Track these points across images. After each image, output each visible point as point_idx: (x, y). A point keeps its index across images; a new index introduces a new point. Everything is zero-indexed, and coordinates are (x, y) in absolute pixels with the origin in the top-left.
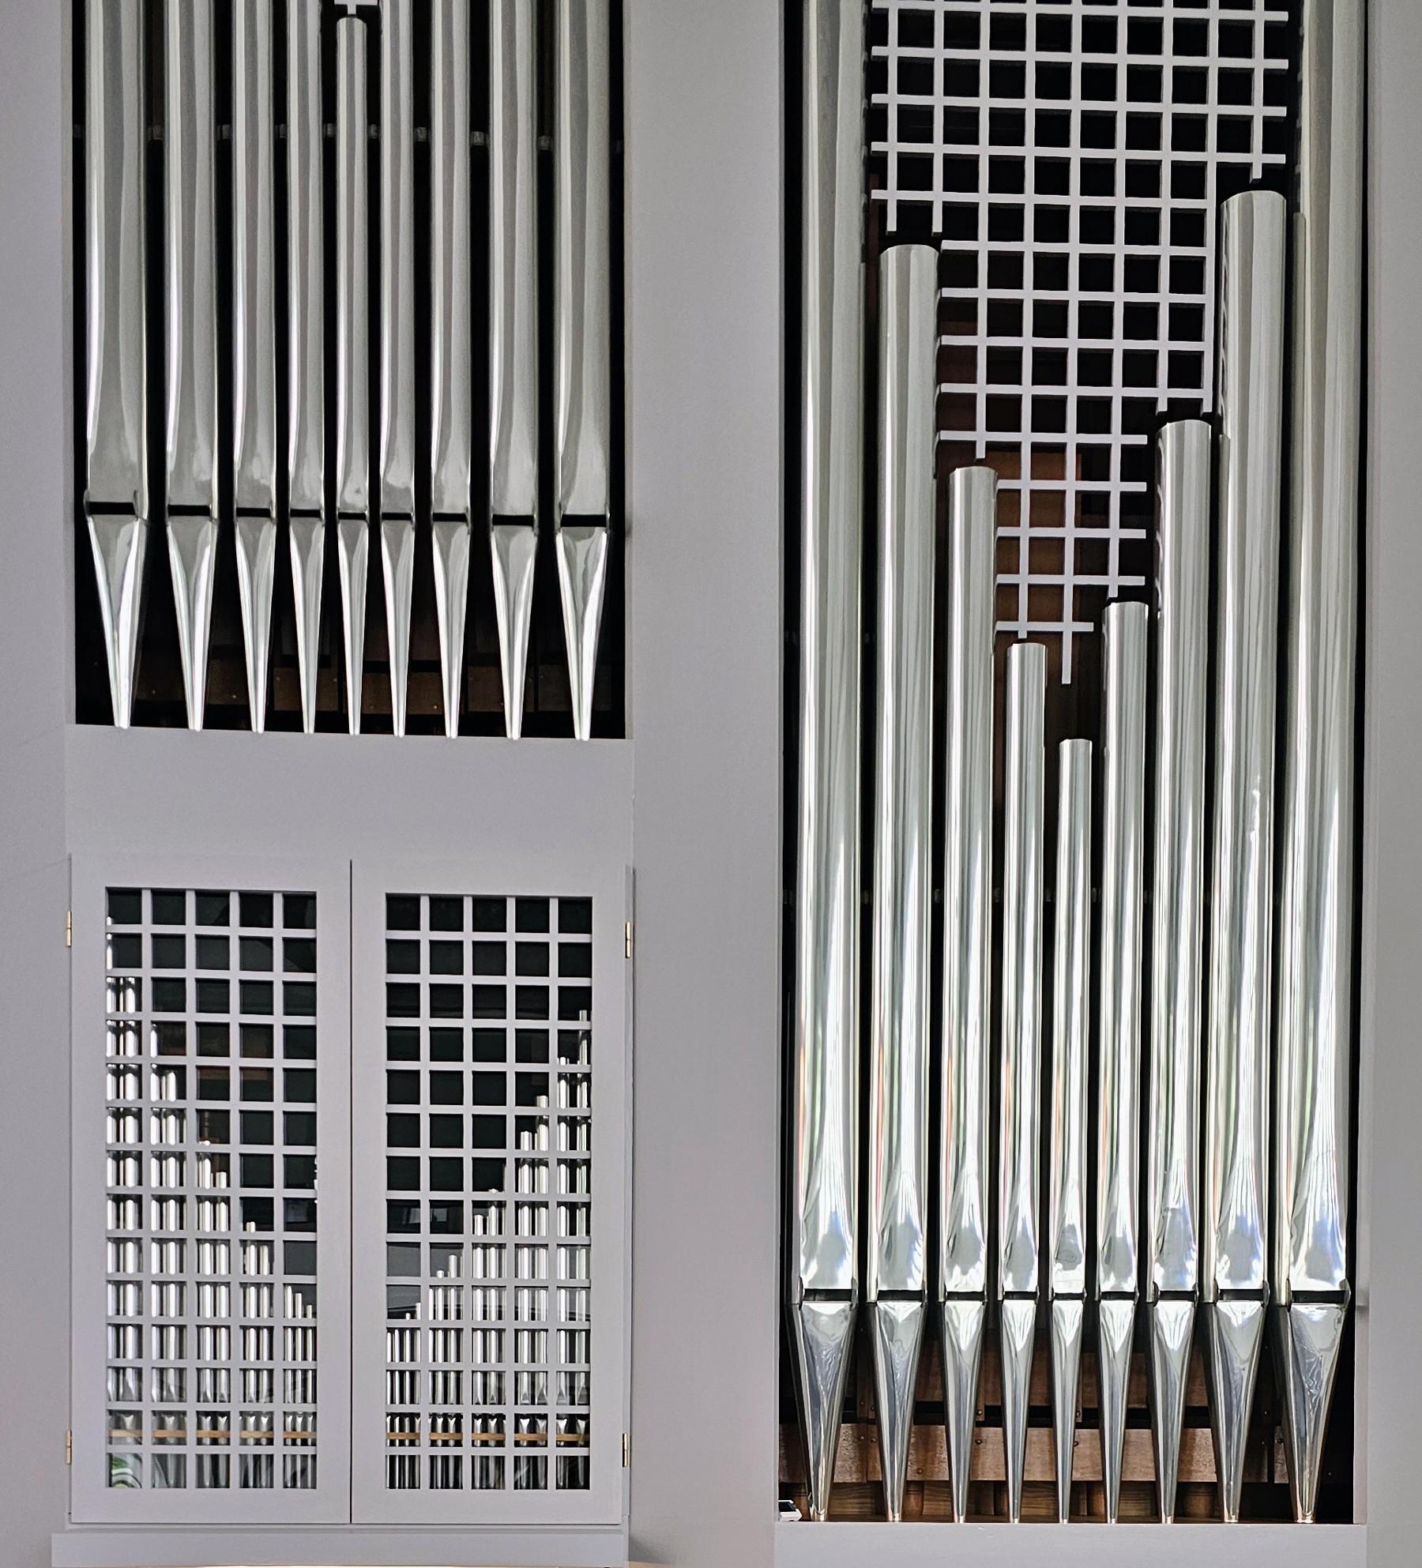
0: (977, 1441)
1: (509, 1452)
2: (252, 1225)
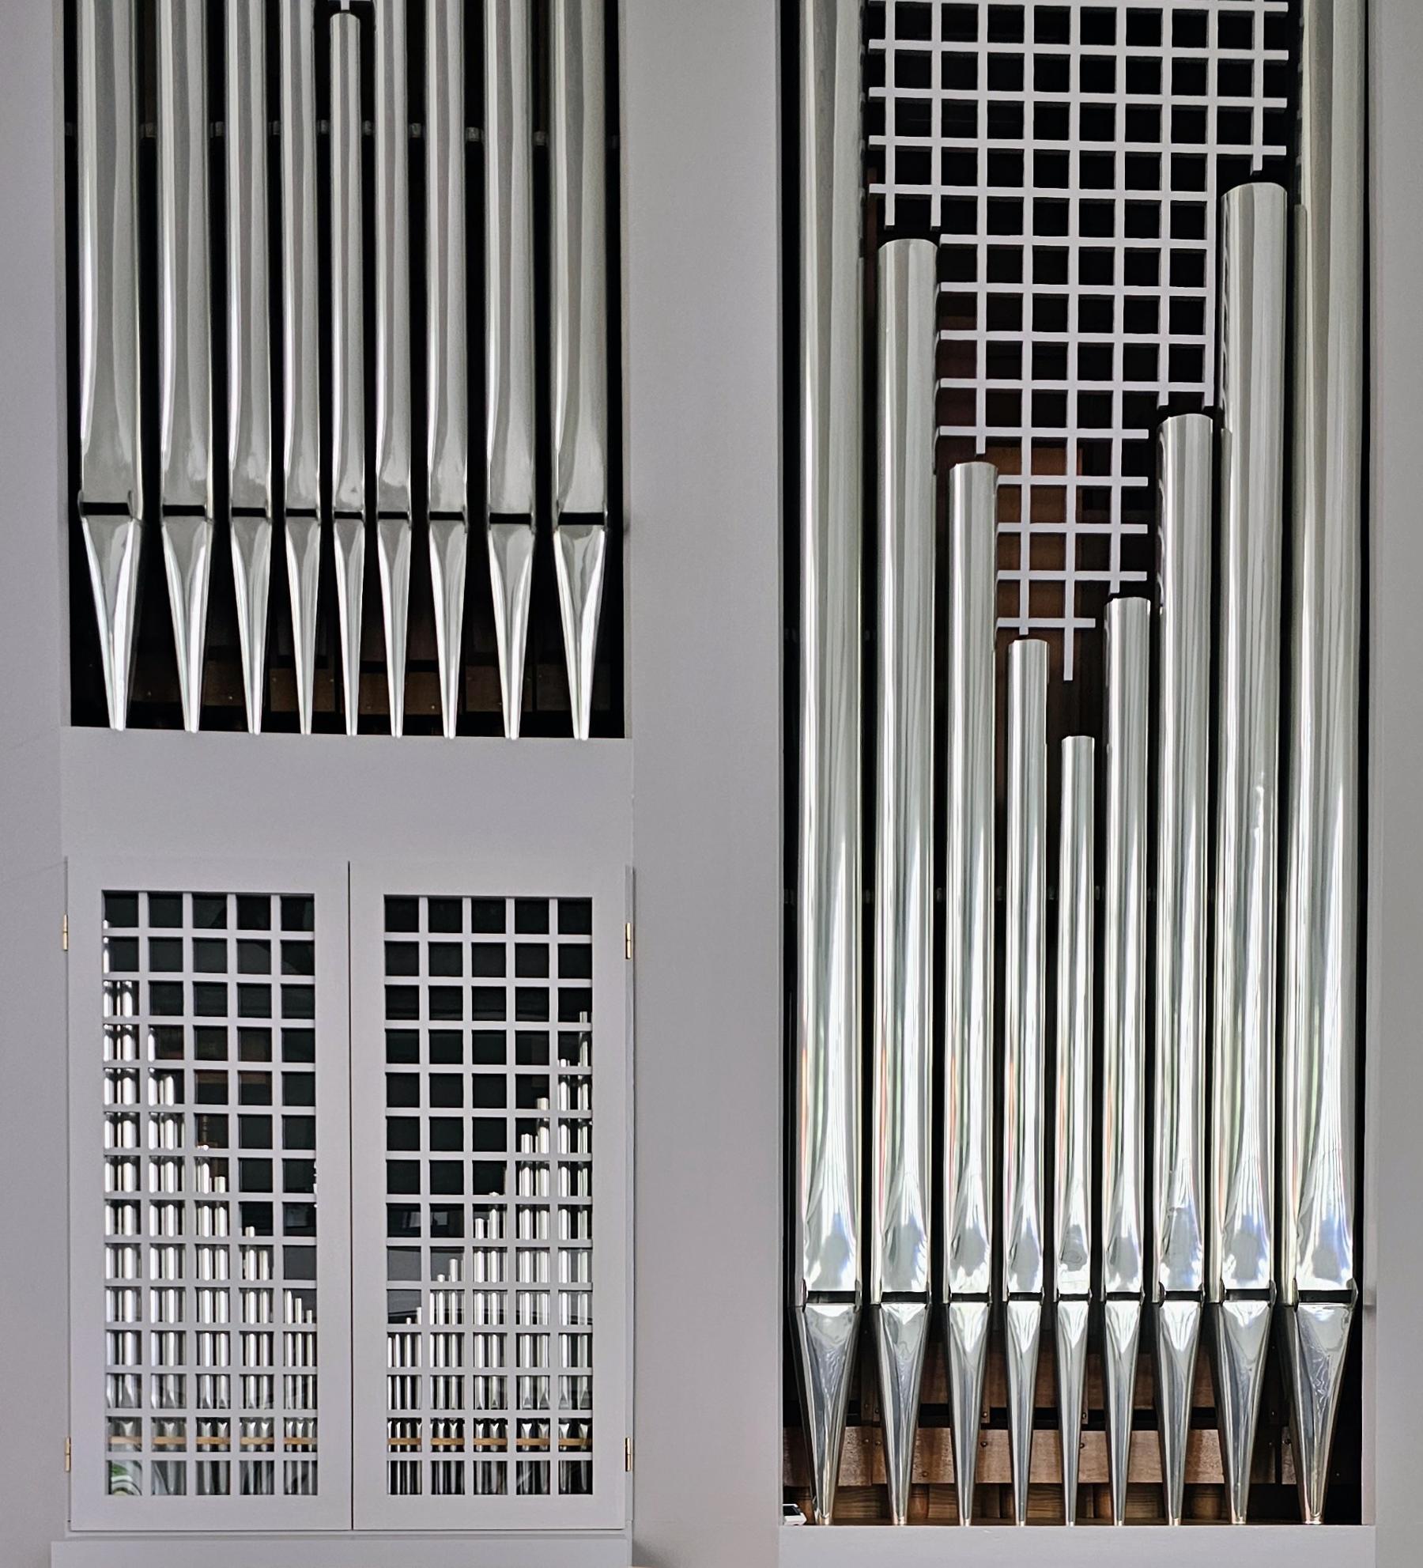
0: (982, 1444)
1: (511, 1457)
2: (251, 1230)
